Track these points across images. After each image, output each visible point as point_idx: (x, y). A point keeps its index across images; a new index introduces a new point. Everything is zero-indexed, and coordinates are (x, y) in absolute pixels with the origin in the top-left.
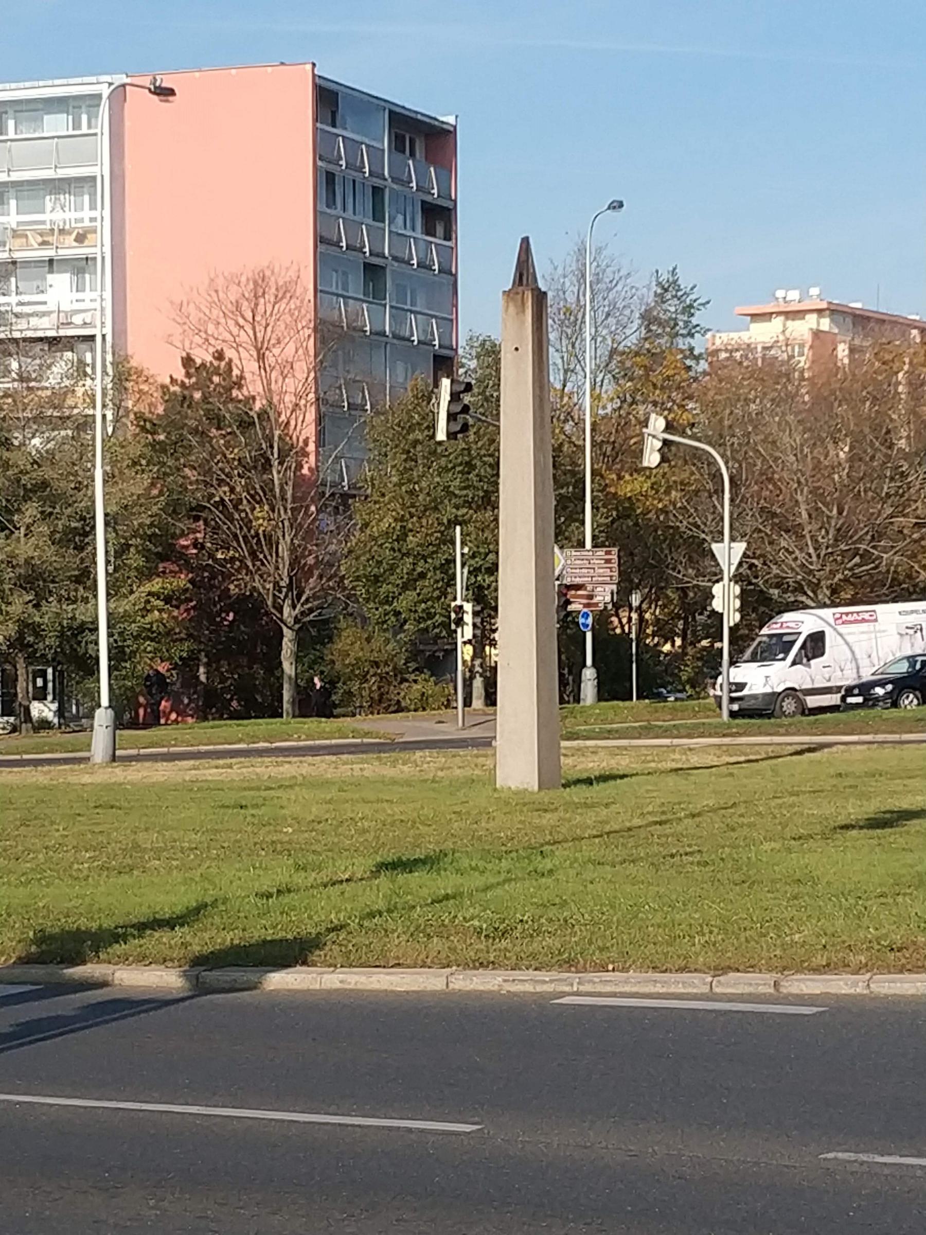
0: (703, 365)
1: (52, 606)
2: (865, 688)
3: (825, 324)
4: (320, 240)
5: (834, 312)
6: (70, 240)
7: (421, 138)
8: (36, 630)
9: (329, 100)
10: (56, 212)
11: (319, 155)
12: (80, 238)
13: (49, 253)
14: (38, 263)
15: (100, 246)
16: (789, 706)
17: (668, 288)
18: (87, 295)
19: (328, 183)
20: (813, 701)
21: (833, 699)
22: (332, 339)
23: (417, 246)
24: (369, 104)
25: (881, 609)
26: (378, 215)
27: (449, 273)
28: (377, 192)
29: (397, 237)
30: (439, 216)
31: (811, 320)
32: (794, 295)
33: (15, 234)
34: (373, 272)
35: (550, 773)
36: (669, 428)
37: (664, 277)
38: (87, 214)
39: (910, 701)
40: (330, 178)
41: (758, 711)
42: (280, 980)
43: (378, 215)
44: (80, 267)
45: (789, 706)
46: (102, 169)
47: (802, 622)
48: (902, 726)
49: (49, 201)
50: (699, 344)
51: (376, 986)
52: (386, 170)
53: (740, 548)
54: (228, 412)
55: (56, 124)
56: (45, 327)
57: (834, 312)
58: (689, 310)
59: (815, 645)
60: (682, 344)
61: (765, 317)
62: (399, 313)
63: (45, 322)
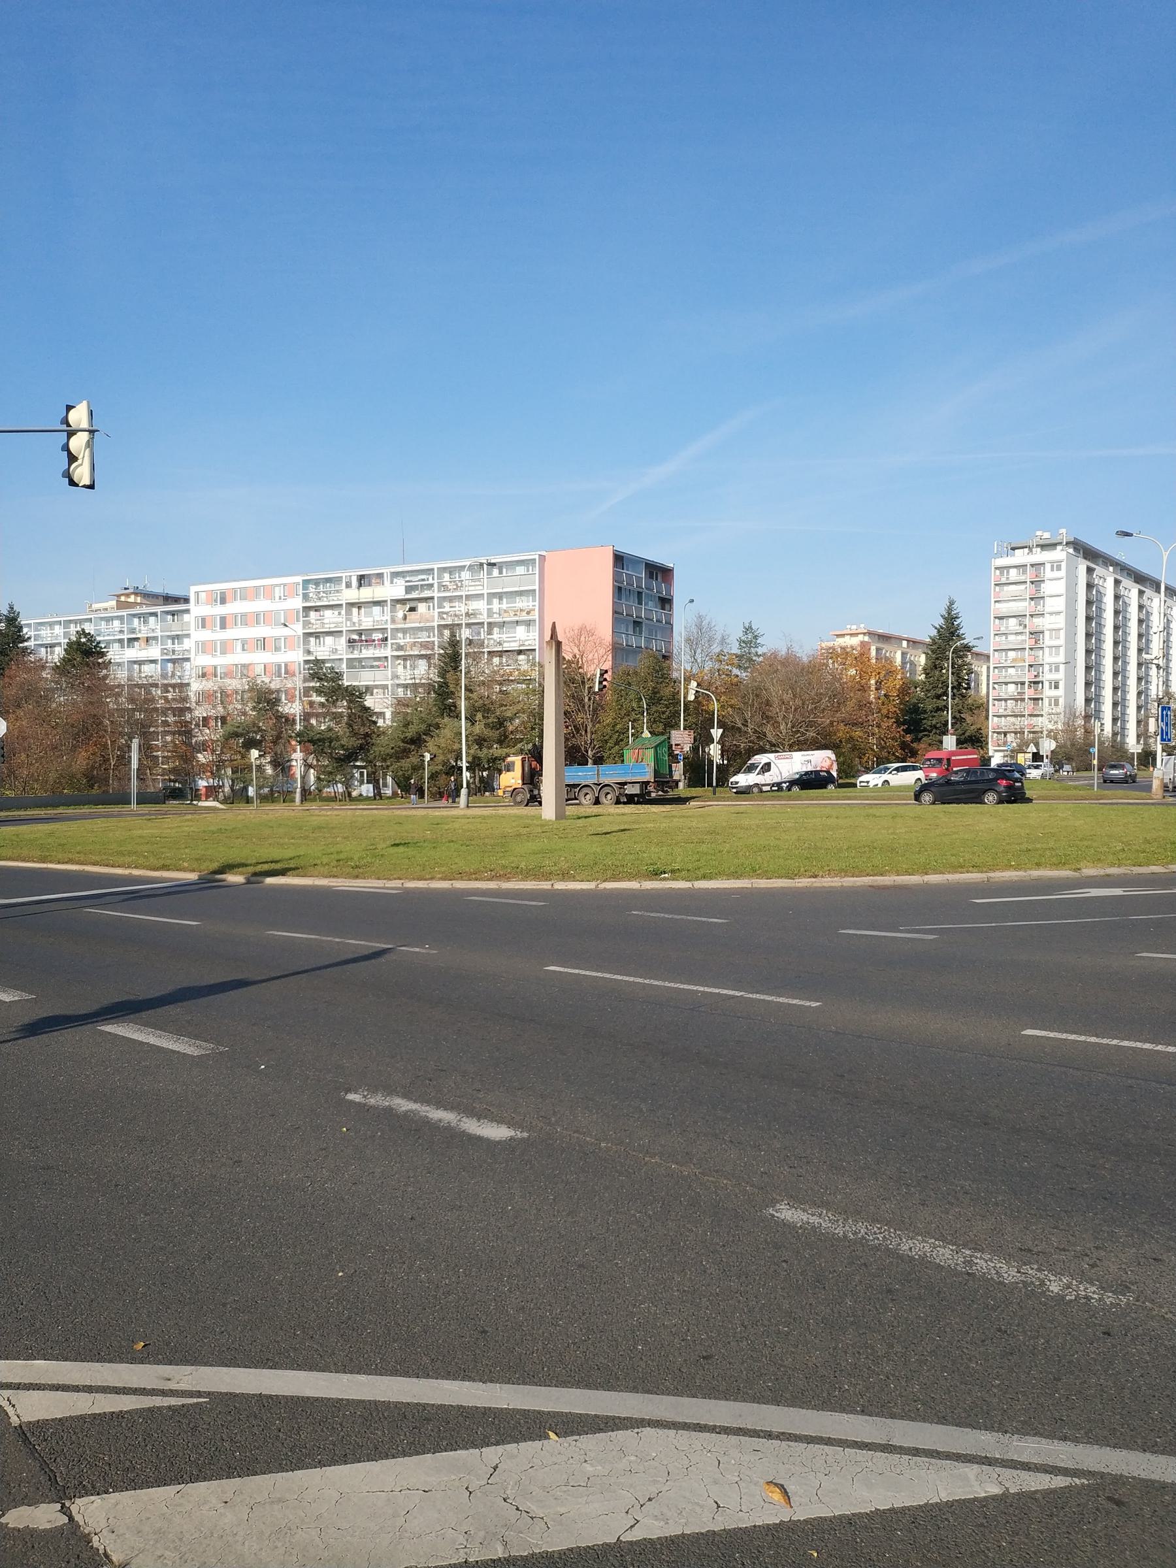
0: (761, 659)
1: (485, 750)
2: (779, 784)
3: (866, 639)
4: (615, 612)
5: (870, 634)
6: (524, 613)
7: (660, 573)
8: (479, 758)
9: (619, 559)
10: (522, 603)
11: (615, 580)
12: (528, 613)
13: (516, 618)
14: (512, 622)
15: (535, 615)
16: (755, 790)
17: (748, 629)
18: (531, 634)
19: (619, 591)
20: (765, 789)
21: (768, 788)
22: (618, 650)
23: (656, 613)
24: (636, 561)
25: (794, 754)
26: (640, 603)
27: (669, 624)
28: (640, 594)
29: (649, 610)
30: (666, 602)
31: (861, 637)
32: (854, 627)
33: (505, 611)
34: (637, 624)
35: (560, 815)
36: (699, 685)
37: (747, 625)
38: (531, 604)
39: (796, 789)
40: (620, 589)
41: (745, 792)
42: (270, 880)
43: (640, 603)
44: (528, 623)
45: (755, 790)
46: (536, 587)
47: (762, 759)
48: (790, 798)
49: (518, 599)
50: (760, 651)
51: (800, 885)
52: (643, 587)
53: (721, 731)
54: (578, 678)
55: (520, 570)
56: (514, 646)
57: (870, 634)
58: (756, 637)
59: (767, 767)
60: (753, 650)
61: (843, 635)
62: (648, 640)
63: (513, 644)
